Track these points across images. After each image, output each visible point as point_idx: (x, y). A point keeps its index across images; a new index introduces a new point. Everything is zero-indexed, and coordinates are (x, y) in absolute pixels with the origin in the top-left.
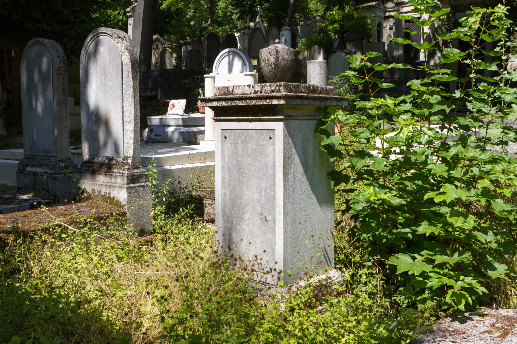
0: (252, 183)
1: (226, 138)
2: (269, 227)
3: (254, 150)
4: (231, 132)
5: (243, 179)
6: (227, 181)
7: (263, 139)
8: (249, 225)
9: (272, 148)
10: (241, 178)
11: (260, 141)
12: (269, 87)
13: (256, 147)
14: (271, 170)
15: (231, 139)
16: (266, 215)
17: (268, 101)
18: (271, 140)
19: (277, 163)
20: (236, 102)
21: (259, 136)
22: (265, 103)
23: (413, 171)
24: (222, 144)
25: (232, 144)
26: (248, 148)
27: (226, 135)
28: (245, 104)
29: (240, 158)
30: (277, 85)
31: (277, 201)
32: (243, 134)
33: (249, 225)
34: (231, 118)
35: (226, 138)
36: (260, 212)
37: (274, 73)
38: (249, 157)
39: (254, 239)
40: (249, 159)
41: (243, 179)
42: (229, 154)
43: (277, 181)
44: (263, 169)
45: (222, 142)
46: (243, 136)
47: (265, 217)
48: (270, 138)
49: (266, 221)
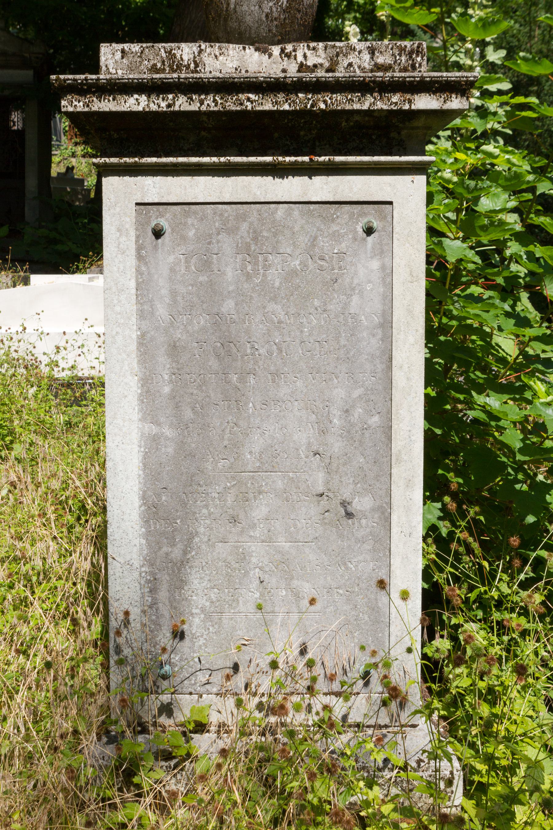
0: (284, 391)
1: (158, 233)
2: (360, 534)
3: (294, 273)
4: (187, 215)
5: (242, 380)
6: (167, 390)
7: (336, 237)
8: (269, 540)
9: (375, 264)
10: (235, 378)
11: (324, 243)
12: (366, 57)
13: (304, 264)
14: (373, 341)
15: (184, 238)
16: (346, 495)
17: (395, 98)
18: (370, 239)
19: (399, 314)
20: (242, 96)
21: (318, 223)
22: (380, 105)
23: (446, 713)
24: (140, 258)
25: (188, 257)
26: (266, 268)
27: (164, 223)
28: (286, 107)
29: (229, 306)
30: (402, 50)
31: (397, 445)
32: (243, 217)
33: (269, 540)
34: (194, 160)
35: (158, 233)
36: (321, 489)
37: (283, 25)
38: (274, 299)
39: (295, 583)
40: (271, 306)
41: (242, 380)
42: (174, 294)
43: (398, 376)
44: (337, 338)
45: (139, 248)
46: (244, 226)
47: (344, 504)
48: (369, 231)
49: (349, 515)
